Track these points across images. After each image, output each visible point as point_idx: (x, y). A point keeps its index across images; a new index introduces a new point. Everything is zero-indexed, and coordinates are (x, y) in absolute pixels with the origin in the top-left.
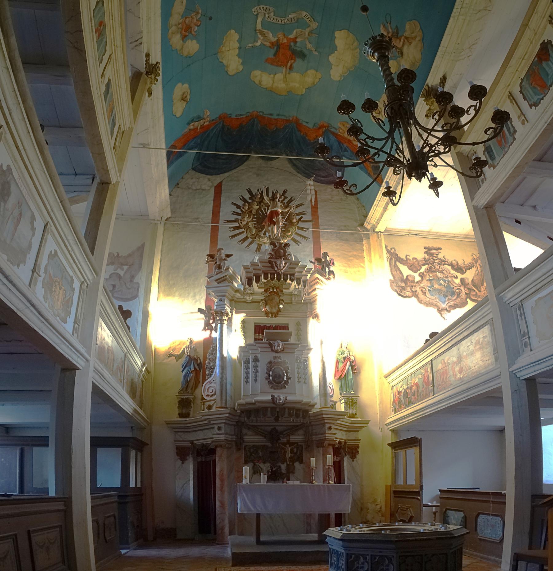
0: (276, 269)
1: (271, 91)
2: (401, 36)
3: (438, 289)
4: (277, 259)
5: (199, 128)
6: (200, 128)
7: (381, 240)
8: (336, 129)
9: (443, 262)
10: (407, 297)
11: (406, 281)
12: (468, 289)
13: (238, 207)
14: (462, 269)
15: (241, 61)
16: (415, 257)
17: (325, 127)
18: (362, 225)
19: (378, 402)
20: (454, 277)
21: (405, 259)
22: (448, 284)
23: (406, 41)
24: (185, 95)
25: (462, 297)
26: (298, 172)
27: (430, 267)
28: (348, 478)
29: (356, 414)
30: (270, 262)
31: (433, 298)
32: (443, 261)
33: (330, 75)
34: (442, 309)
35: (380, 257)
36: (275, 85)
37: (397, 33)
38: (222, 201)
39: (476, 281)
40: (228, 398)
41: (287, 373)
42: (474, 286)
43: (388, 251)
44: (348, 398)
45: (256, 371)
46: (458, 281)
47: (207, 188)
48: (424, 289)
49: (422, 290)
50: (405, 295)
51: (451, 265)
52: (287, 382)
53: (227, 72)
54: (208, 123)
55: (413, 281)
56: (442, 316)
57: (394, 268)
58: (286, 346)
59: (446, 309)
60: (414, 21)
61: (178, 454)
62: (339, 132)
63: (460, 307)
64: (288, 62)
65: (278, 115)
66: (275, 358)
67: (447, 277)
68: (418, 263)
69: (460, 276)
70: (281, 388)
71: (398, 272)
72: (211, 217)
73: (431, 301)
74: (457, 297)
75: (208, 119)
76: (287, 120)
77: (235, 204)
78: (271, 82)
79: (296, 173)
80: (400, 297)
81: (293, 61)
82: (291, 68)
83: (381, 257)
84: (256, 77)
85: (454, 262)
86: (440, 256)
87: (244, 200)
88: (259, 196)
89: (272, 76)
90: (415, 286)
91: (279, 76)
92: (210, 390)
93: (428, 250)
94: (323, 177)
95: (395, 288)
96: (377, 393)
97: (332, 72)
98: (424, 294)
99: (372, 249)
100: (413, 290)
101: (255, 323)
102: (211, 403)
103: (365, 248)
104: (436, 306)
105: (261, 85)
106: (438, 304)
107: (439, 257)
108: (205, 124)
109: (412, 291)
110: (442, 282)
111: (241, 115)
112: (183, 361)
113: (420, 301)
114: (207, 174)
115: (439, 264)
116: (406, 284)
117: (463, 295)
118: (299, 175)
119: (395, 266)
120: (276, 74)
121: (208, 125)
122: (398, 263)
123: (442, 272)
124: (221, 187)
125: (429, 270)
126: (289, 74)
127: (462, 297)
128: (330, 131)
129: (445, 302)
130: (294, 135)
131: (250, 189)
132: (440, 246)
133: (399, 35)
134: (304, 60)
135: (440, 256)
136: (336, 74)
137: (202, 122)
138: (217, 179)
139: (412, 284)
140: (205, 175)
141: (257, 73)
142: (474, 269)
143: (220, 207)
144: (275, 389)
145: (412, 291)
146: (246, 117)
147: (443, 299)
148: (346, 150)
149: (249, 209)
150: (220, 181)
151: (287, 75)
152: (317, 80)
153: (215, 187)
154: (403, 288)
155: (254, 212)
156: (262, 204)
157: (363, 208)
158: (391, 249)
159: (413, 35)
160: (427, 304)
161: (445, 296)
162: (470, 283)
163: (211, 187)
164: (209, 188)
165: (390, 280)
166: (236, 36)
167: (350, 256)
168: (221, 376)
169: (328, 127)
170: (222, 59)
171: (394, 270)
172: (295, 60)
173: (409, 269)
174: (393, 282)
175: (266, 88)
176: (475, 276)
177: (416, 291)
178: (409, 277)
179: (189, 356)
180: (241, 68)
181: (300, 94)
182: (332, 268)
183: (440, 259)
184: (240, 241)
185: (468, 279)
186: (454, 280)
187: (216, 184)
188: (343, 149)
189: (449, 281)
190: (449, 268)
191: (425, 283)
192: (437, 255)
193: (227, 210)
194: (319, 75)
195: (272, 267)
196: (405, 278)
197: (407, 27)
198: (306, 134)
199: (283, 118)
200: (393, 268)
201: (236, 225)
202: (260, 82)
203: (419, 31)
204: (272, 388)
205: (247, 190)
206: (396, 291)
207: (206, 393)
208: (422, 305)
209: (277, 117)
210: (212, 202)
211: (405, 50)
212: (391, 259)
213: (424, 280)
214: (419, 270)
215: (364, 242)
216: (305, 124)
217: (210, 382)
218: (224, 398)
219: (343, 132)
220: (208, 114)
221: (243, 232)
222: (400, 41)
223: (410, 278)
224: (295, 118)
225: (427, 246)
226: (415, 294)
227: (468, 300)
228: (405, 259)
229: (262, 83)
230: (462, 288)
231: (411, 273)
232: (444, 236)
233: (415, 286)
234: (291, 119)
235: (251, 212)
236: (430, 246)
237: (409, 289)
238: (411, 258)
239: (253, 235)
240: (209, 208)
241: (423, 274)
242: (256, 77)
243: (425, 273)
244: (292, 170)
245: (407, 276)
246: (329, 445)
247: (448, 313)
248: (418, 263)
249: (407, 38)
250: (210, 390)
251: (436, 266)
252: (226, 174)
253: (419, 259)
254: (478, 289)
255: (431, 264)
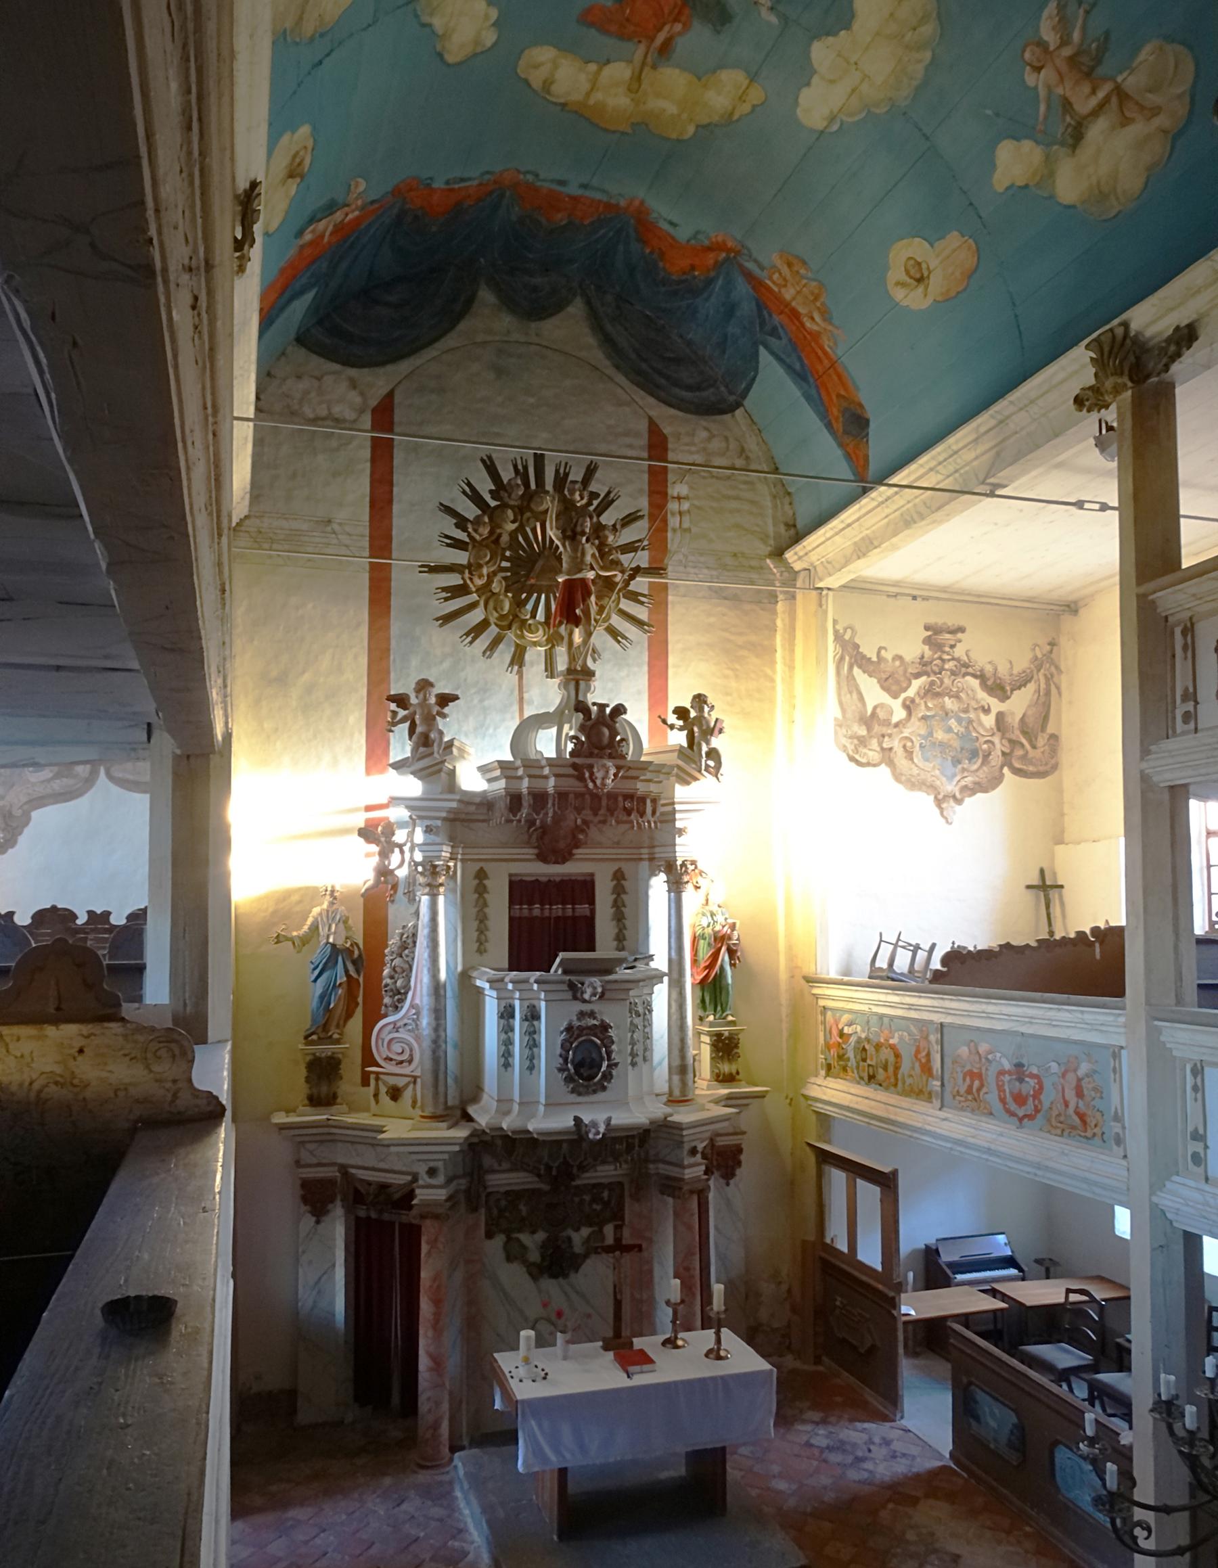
0: (591, 785)
1: (579, 118)
2: (1105, 79)
3: (941, 744)
4: (591, 755)
5: (327, 234)
6: (331, 234)
7: (826, 612)
8: (762, 268)
9: (964, 668)
10: (868, 764)
11: (870, 720)
12: (1011, 741)
13: (462, 523)
14: (1002, 689)
15: (494, 14)
16: (900, 653)
17: (729, 250)
18: (778, 553)
19: (785, 1034)
20: (983, 707)
21: (875, 659)
22: (967, 728)
23: (1114, 100)
24: (298, 160)
25: (993, 763)
26: (617, 367)
27: (932, 683)
28: (716, 1228)
29: (738, 1073)
30: (574, 766)
31: (928, 766)
32: (966, 666)
33: (796, 103)
34: (945, 797)
35: (818, 662)
36: (598, 96)
37: (1098, 60)
38: (396, 462)
39: (1030, 721)
40: (450, 1081)
41: (609, 1053)
42: (1024, 733)
43: (838, 637)
44: (719, 1035)
45: (533, 1044)
46: (989, 721)
47: (349, 415)
48: (909, 744)
49: (904, 747)
50: (864, 761)
51: (981, 677)
52: (608, 1076)
53: (440, 55)
54: (357, 213)
55: (887, 723)
56: (942, 814)
57: (848, 684)
58: (608, 987)
59: (954, 797)
60: (1179, 48)
61: (305, 1199)
62: (771, 278)
63: (986, 791)
64: (660, 30)
65: (584, 186)
66: (582, 1015)
67: (966, 711)
68: (905, 672)
69: (996, 705)
70: (595, 1092)
71: (855, 696)
72: (367, 518)
73: (923, 777)
74: (983, 764)
75: (359, 202)
76: (608, 206)
77: (449, 511)
78: (586, 86)
79: (611, 371)
80: (853, 764)
81: (678, 27)
82: (665, 50)
83: (820, 660)
84: (537, 66)
85: (989, 669)
86: (959, 651)
87: (476, 497)
88: (521, 493)
89: (593, 67)
90: (890, 736)
91: (619, 71)
92: (397, 1047)
93: (935, 636)
94: (689, 388)
95: (844, 741)
96: (784, 1011)
97: (806, 96)
98: (909, 754)
99: (799, 634)
100: (885, 746)
101: (510, 875)
102: (401, 1082)
103: (779, 623)
104: (931, 788)
105: (549, 92)
106: (938, 783)
107: (956, 655)
108: (350, 216)
109: (883, 749)
110: (953, 723)
111: (462, 180)
112: (317, 954)
113: (897, 777)
114: (347, 363)
115: (953, 673)
116: (869, 729)
117: (996, 759)
118: (621, 379)
119: (851, 677)
120: (608, 62)
121: (357, 220)
122: (856, 670)
123: (957, 697)
124: (392, 410)
125: (929, 692)
126: (654, 67)
127: (993, 763)
128: (741, 266)
129: (954, 775)
130: (621, 247)
131: (490, 458)
132: (962, 623)
133: (1101, 71)
134: (718, 32)
135: (959, 651)
136: (818, 105)
137: (338, 216)
138: (379, 381)
139: (885, 730)
140: (337, 367)
141: (544, 54)
142: (1031, 687)
143: (391, 484)
144: (580, 1094)
145: (883, 749)
146: (480, 184)
147: (950, 770)
148: (774, 332)
149: (491, 532)
150: (383, 391)
151: (647, 69)
152: (746, 108)
153: (374, 411)
154: (862, 742)
155: (505, 539)
156: (528, 514)
157: (787, 500)
158: (845, 630)
159: (1153, 99)
160: (913, 784)
161: (956, 761)
162: (1016, 724)
163: (362, 411)
164: (353, 416)
165: (836, 719)
166: (1187, 1426)
167: (741, 647)
168: (433, 1036)
169: (738, 253)
170: (431, 14)
171: (845, 689)
172: (687, 27)
173: (883, 688)
174: (840, 726)
175: (564, 105)
176: (1029, 706)
177: (891, 749)
178: (878, 710)
179: (333, 945)
180: (490, 38)
181: (674, 136)
182: (715, 742)
183: (958, 660)
184: (467, 634)
185: (1013, 714)
186: (982, 716)
187: (373, 403)
188: (768, 328)
189: (970, 722)
190: (975, 683)
191: (915, 729)
192: (952, 647)
193: (420, 529)
194: (756, 95)
195: (581, 778)
196: (869, 712)
197: (1146, 54)
198: (662, 254)
199: (598, 196)
200: (844, 684)
201: (454, 580)
202: (547, 84)
203: (1180, 96)
204: (573, 1091)
205: (483, 461)
206: (845, 749)
207: (385, 1053)
208: (900, 787)
209: (579, 192)
210: (368, 464)
211: (1096, 131)
212: (842, 659)
213: (913, 719)
214: (905, 690)
215: (780, 607)
216: (665, 226)
217: (395, 1023)
218: (441, 1089)
219: (780, 281)
220: (362, 188)
221: (473, 606)
222: (1094, 92)
223: (881, 714)
224: (637, 203)
225: (932, 620)
226: (887, 755)
227: (1006, 770)
228: (875, 659)
229: (554, 88)
230: (996, 740)
231: (885, 698)
232: (979, 596)
233: (890, 736)
234: (623, 203)
235: (497, 541)
236: (940, 621)
237: (874, 743)
238: (888, 655)
239: (502, 617)
240: (360, 486)
241: (913, 701)
242: (537, 66)
243: (917, 700)
244: (598, 356)
245: (875, 708)
246: (692, 1192)
247: (957, 808)
248: (905, 672)
249: (1121, 94)
250: (397, 1047)
251: (946, 681)
252: (404, 366)
253: (908, 658)
254: (1030, 742)
255: (935, 673)
